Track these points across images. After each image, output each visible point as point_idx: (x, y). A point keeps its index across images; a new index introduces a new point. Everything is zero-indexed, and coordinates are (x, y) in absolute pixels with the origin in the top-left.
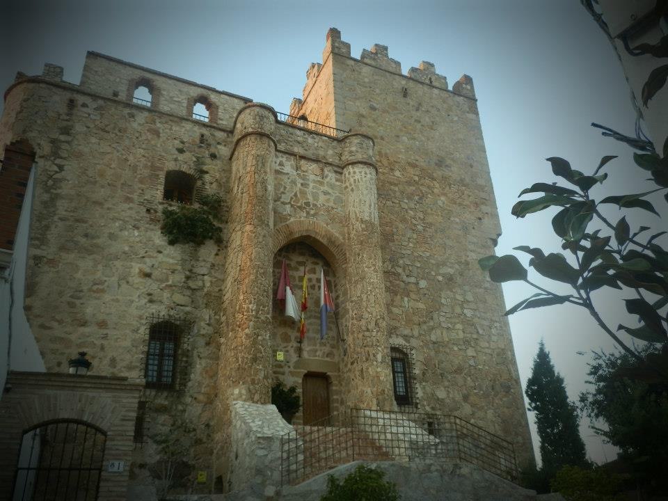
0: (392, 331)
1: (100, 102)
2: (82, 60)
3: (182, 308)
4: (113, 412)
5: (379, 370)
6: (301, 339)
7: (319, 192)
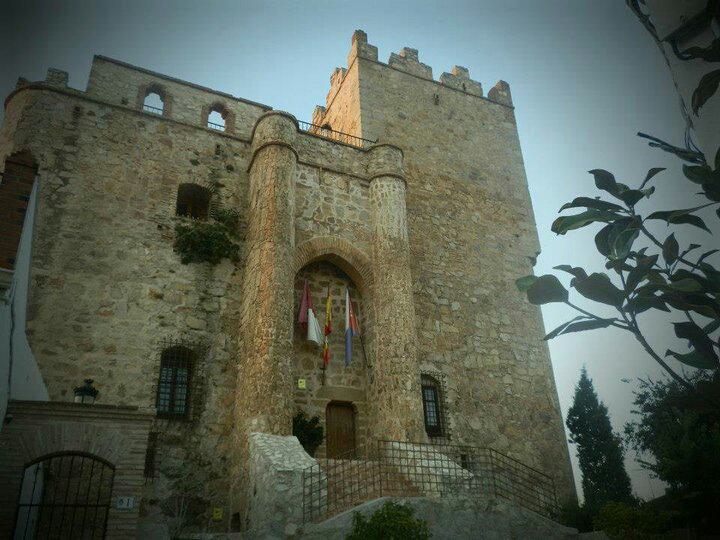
0: (422, 357)
1: (108, 110)
2: (89, 65)
4: (122, 444)
5: (408, 398)
7: (344, 207)
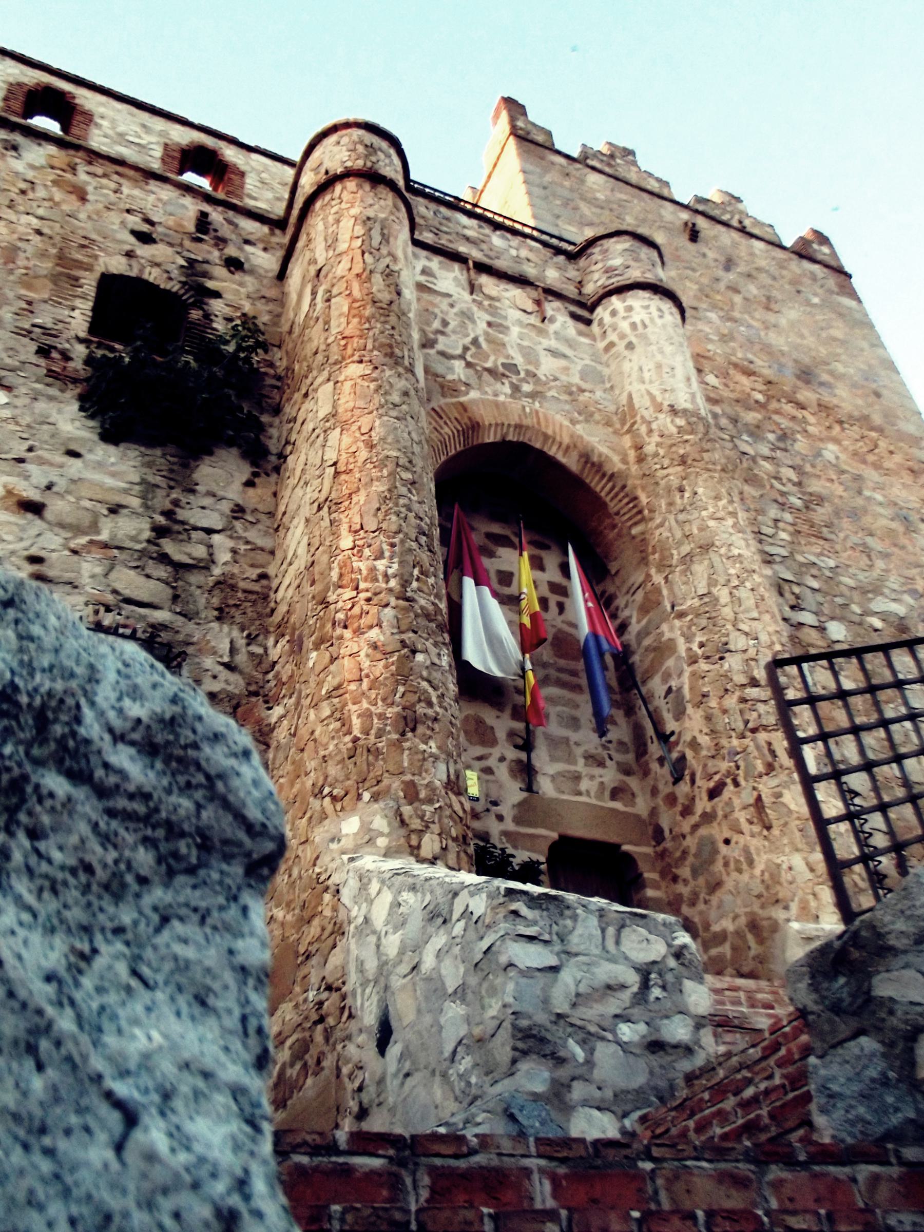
3: (142, 611)
7: (539, 349)
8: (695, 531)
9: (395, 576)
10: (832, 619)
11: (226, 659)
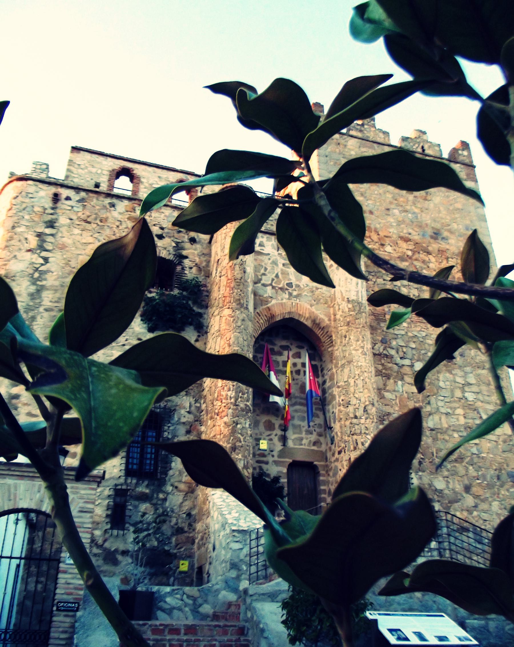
1: (83, 194)
6: (285, 427)
8: (347, 355)
9: (233, 397)
10: (418, 361)
11: (188, 410)
